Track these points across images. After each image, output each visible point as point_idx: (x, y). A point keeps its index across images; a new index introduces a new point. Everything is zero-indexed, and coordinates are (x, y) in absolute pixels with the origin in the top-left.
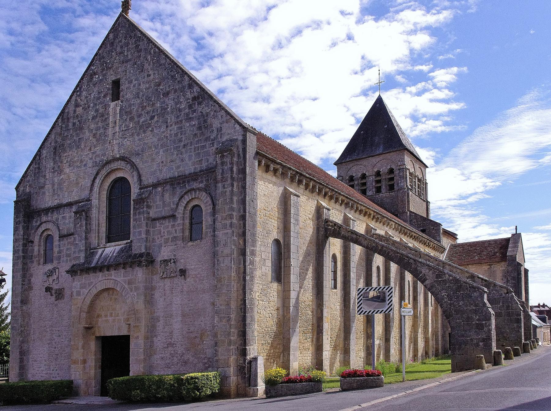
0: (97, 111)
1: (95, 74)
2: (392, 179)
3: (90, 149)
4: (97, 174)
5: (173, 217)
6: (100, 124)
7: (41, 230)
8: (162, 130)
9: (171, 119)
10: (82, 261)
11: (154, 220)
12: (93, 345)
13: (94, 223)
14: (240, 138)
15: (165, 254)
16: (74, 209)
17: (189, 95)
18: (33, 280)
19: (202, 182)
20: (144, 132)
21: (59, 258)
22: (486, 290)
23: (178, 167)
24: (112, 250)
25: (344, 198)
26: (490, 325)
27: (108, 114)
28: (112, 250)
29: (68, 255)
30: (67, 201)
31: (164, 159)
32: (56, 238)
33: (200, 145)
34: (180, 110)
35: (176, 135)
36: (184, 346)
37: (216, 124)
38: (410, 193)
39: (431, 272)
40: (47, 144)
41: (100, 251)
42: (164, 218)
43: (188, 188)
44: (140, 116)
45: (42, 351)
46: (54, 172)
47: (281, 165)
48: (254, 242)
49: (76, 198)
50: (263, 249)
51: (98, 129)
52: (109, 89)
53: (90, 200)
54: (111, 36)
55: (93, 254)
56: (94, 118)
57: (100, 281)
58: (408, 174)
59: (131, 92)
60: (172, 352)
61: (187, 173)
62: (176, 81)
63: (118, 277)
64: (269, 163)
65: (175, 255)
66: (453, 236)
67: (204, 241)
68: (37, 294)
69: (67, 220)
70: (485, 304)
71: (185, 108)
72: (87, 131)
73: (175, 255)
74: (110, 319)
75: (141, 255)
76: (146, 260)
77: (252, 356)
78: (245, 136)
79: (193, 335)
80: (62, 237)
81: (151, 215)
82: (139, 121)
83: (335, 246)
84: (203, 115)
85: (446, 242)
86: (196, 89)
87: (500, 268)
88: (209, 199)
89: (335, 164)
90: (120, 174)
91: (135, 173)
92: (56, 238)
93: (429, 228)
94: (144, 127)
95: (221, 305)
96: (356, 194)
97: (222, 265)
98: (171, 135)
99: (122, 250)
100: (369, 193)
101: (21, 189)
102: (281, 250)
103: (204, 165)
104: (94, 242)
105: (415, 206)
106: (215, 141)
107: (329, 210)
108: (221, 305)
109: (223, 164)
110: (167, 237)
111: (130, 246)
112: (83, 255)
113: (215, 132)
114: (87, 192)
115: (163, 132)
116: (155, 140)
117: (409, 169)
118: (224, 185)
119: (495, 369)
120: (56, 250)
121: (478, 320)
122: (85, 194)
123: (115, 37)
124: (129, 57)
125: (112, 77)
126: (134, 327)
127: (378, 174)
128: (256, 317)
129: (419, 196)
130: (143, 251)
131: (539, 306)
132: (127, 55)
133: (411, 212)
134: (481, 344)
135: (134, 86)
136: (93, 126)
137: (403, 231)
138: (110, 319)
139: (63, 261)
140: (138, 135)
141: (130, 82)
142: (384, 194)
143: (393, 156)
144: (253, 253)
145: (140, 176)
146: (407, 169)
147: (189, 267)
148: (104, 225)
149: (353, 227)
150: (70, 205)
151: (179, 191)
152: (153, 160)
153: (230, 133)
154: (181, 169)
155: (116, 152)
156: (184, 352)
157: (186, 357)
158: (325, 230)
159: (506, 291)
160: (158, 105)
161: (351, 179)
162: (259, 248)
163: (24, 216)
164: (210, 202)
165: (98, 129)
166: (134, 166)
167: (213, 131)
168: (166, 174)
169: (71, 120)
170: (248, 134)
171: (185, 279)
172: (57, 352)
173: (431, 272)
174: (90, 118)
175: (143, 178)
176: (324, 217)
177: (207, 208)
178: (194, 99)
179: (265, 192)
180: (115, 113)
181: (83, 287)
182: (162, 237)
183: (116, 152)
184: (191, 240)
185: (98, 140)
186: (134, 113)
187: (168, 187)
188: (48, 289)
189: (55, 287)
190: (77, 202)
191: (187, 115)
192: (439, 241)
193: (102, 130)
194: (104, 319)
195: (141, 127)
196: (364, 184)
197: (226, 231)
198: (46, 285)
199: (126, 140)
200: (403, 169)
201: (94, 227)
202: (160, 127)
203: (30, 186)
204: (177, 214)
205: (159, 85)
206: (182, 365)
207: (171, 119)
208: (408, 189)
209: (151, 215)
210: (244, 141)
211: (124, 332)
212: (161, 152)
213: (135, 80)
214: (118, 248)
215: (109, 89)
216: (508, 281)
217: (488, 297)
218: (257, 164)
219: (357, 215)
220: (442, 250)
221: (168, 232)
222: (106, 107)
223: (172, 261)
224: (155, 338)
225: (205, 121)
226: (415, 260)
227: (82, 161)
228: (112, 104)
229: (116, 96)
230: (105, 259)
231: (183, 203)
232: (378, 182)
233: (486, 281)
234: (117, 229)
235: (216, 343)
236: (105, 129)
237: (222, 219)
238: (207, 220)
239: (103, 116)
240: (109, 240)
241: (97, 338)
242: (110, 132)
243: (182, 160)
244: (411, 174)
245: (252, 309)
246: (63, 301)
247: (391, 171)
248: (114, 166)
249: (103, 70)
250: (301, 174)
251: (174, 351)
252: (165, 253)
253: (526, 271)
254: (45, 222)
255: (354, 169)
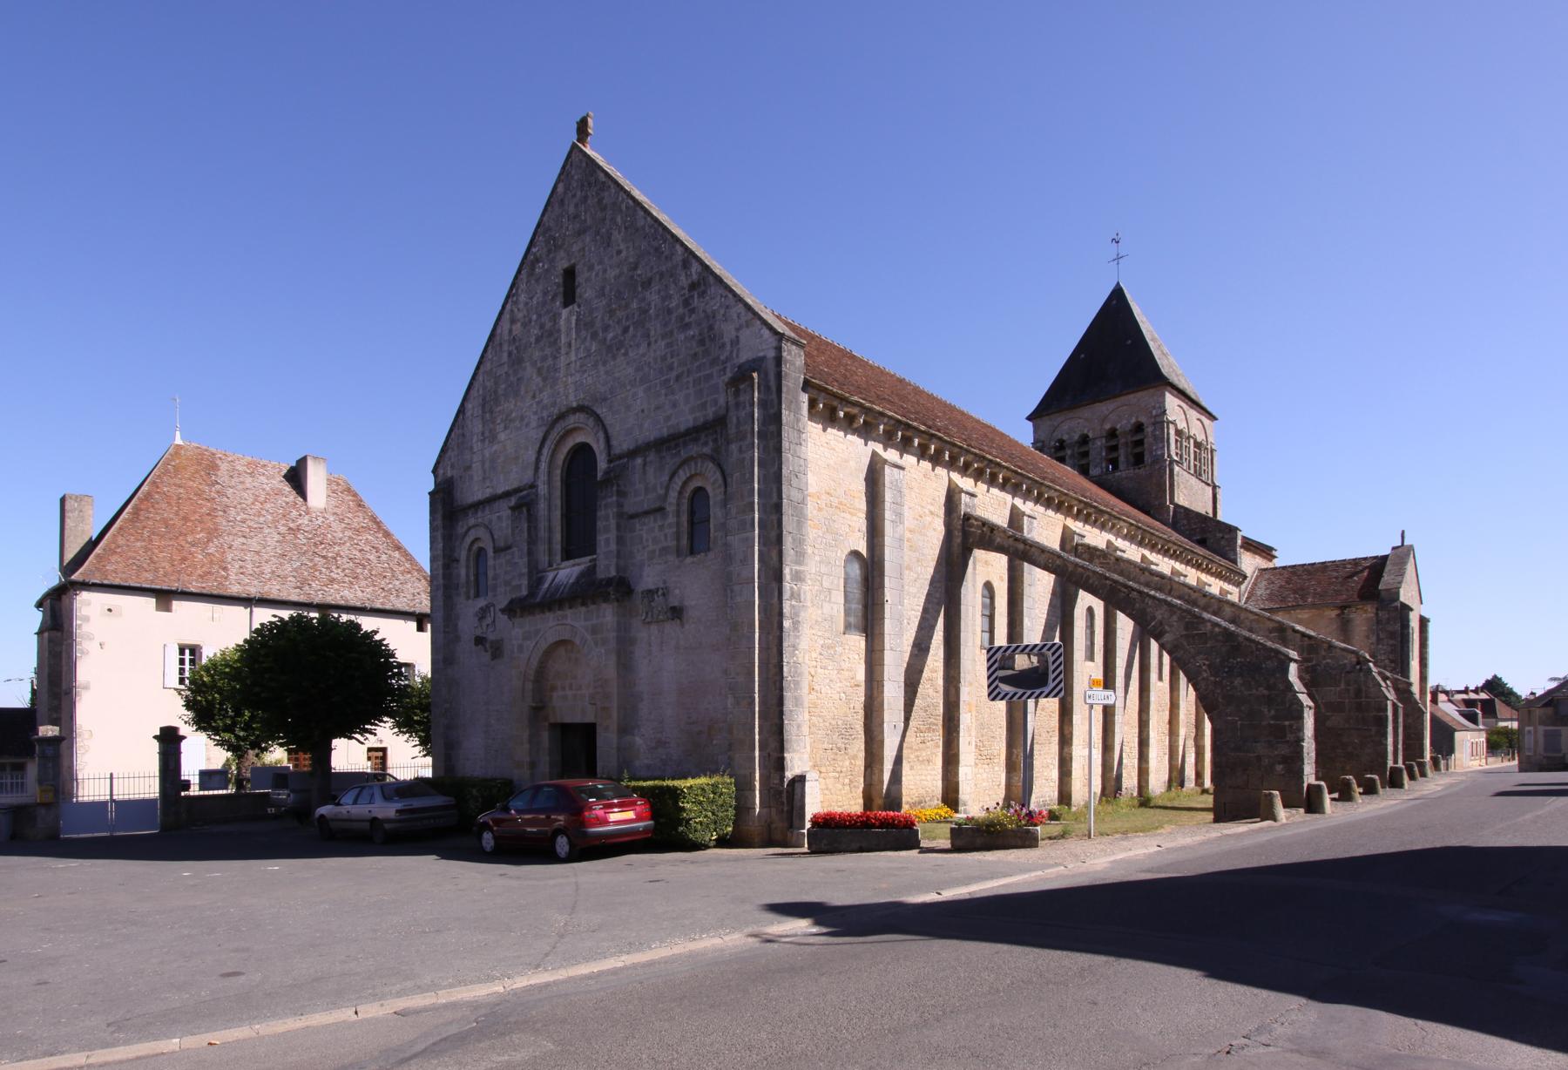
0: (542, 327)
1: (537, 260)
2: (1140, 443)
3: (534, 397)
6: (548, 351)
7: (469, 540)
9: (655, 328)
10: (525, 593)
11: (632, 517)
12: (545, 736)
13: (543, 525)
14: (771, 354)
16: (513, 501)
17: (684, 281)
18: (460, 624)
19: (706, 444)
22: (1293, 654)
23: (668, 418)
24: (567, 573)
25: (1009, 474)
26: (1301, 729)
27: (559, 331)
29: (507, 583)
32: (490, 553)
34: (669, 312)
35: (664, 358)
37: (728, 330)
38: (1177, 469)
39: (1175, 618)
40: (474, 393)
41: (551, 576)
42: (647, 513)
43: (684, 455)
44: (606, 328)
46: (483, 441)
47: (861, 406)
48: (800, 556)
49: (515, 485)
50: (824, 569)
51: (544, 359)
52: (558, 285)
54: (560, 188)
55: (540, 581)
56: (538, 340)
57: (550, 626)
58: (1172, 432)
61: (682, 428)
63: (575, 621)
64: (835, 403)
66: (1265, 551)
67: (711, 555)
68: (466, 646)
70: (1290, 685)
74: (569, 693)
75: (609, 581)
76: (620, 589)
77: (797, 771)
78: (779, 349)
81: (626, 509)
83: (988, 567)
84: (707, 317)
85: (1249, 563)
86: (695, 267)
87: (1362, 618)
88: (718, 474)
89: (1029, 418)
90: (580, 438)
91: (601, 435)
92: (490, 553)
93: (1211, 538)
94: (612, 349)
96: (1067, 473)
97: (739, 599)
98: (655, 359)
99: (582, 575)
100: (1094, 472)
101: (441, 472)
102: (870, 573)
103: (710, 412)
104: (543, 559)
105: (1189, 493)
107: (973, 495)
109: (737, 405)
110: (651, 548)
111: (595, 566)
112: (525, 582)
113: (728, 347)
114: (530, 473)
115: (643, 355)
116: (630, 370)
117: (1173, 423)
120: (490, 574)
121: (1273, 718)
122: (528, 476)
123: (567, 189)
124: (589, 222)
125: (563, 264)
127: (1112, 434)
128: (807, 698)
129: (1198, 474)
130: (613, 573)
131: (1466, 691)
133: (1177, 506)
134: (1279, 768)
136: (537, 354)
137: (1140, 537)
138: (569, 693)
140: (604, 364)
141: (591, 268)
142: (1125, 473)
143: (1142, 398)
144: (798, 577)
145: (608, 439)
146: (1169, 422)
148: (559, 528)
149: (1030, 531)
150: (507, 494)
151: (671, 462)
152: (628, 408)
153: (753, 346)
154: (673, 422)
155: (571, 398)
158: (964, 536)
159: (1354, 660)
160: (635, 305)
161: (1061, 445)
162: (811, 567)
163: (444, 517)
164: (720, 481)
165: (544, 359)
166: (599, 419)
167: (723, 345)
168: (650, 432)
169: (505, 347)
170: (786, 346)
171: (682, 625)
173: (1175, 618)
174: (533, 340)
175: (614, 443)
176: (963, 509)
177: (715, 493)
178: (693, 286)
179: (826, 463)
180: (569, 329)
181: (526, 637)
183: (571, 398)
184: (692, 552)
185: (545, 380)
186: (598, 324)
187: (652, 456)
188: (480, 641)
189: (491, 637)
190: (517, 490)
191: (682, 318)
192: (1235, 562)
193: (550, 361)
194: (561, 693)
195: (609, 348)
196: (1085, 454)
198: (479, 632)
200: (1160, 420)
201: (543, 534)
202: (638, 346)
203: (452, 466)
205: (635, 268)
207: (655, 328)
208: (1172, 462)
209: (626, 509)
210: (779, 360)
211: (589, 719)
212: (641, 394)
214: (577, 570)
215: (558, 285)
216: (1379, 640)
217: (1300, 670)
218: (805, 406)
219: (1040, 509)
220: (1237, 577)
222: (555, 318)
225: (711, 328)
226: (1140, 592)
227: (522, 418)
228: (565, 312)
229: (569, 297)
230: (557, 588)
232: (1114, 448)
233: (1310, 637)
234: (578, 541)
235: (730, 745)
236: (555, 358)
238: (716, 513)
239: (550, 336)
240: (568, 555)
241: (554, 726)
242: (563, 361)
243: (674, 405)
244: (1179, 433)
245: (797, 683)
247: (1139, 428)
248: (572, 420)
249: (549, 251)
250: (909, 426)
252: (648, 578)
253: (1424, 622)
255: (1065, 427)
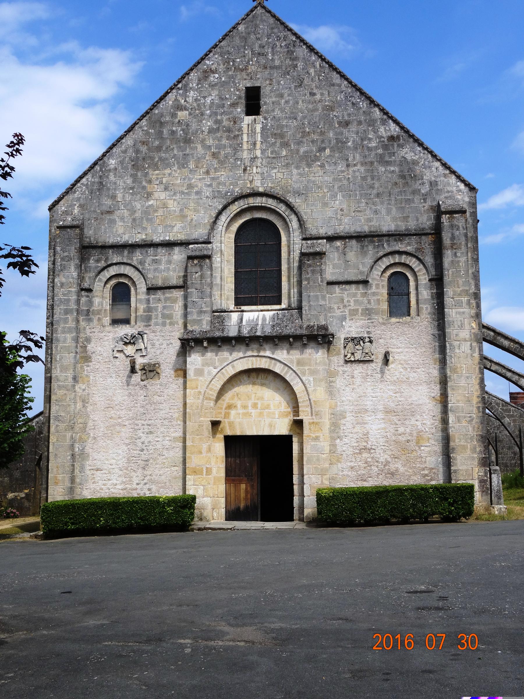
0: (217, 122)
3: (207, 173)
4: (225, 208)
5: (365, 282)
8: (339, 169)
15: (351, 329)
20: (309, 166)
21: (148, 319)
23: (370, 220)
27: (240, 129)
28: (258, 317)
30: (162, 239)
31: (345, 206)
33: (403, 197)
36: (390, 453)
43: (388, 249)
45: (114, 455)
53: (210, 243)
59: (282, 110)
60: (369, 460)
62: (361, 111)
65: (368, 332)
69: (169, 266)
71: (376, 148)
72: (199, 147)
73: (368, 332)
74: (254, 412)
79: (402, 439)
80: (152, 289)
82: (298, 151)
95: (458, 401)
98: (355, 177)
101: (62, 207)
106: (428, 197)
108: (458, 401)
118: (456, 253)
119: (37, 544)
122: (200, 233)
125: (244, 83)
126: (310, 424)
132: (273, 60)
135: (287, 102)
139: (156, 324)
147: (393, 350)
156: (389, 460)
157: (392, 467)
172: (144, 457)
174: (206, 129)
182: (345, 306)
191: (381, 156)
197: (462, 310)
199: (275, 171)
204: (370, 280)
206: (387, 477)
213: (289, 95)
221: (356, 301)
223: (367, 340)
224: (338, 440)
228: (248, 119)
231: (380, 266)
237: (454, 295)
246: (158, 382)
251: (373, 458)
254: (116, 264)
